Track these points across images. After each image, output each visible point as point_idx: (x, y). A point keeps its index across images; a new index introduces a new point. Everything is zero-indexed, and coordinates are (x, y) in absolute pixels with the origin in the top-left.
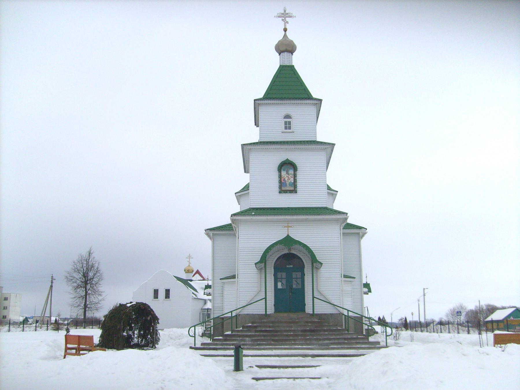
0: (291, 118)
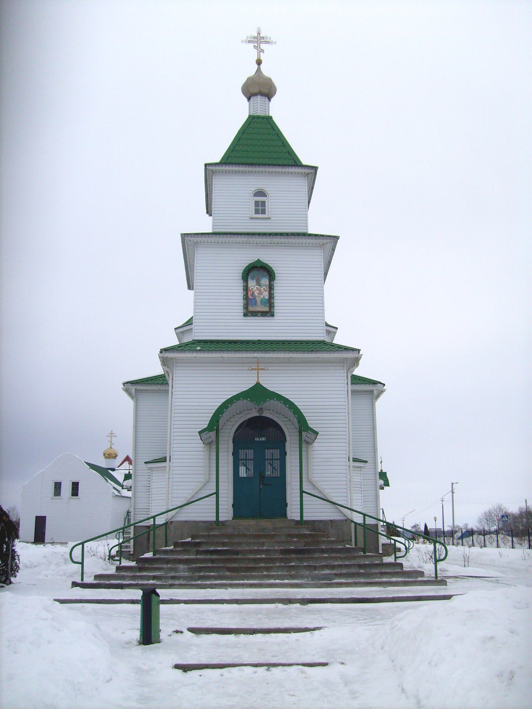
0: (267, 197)
